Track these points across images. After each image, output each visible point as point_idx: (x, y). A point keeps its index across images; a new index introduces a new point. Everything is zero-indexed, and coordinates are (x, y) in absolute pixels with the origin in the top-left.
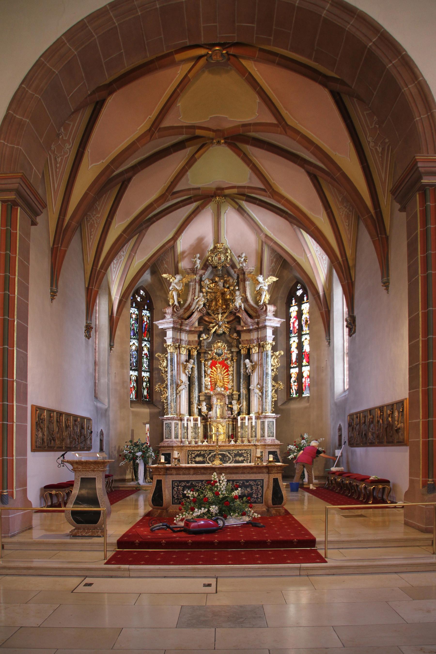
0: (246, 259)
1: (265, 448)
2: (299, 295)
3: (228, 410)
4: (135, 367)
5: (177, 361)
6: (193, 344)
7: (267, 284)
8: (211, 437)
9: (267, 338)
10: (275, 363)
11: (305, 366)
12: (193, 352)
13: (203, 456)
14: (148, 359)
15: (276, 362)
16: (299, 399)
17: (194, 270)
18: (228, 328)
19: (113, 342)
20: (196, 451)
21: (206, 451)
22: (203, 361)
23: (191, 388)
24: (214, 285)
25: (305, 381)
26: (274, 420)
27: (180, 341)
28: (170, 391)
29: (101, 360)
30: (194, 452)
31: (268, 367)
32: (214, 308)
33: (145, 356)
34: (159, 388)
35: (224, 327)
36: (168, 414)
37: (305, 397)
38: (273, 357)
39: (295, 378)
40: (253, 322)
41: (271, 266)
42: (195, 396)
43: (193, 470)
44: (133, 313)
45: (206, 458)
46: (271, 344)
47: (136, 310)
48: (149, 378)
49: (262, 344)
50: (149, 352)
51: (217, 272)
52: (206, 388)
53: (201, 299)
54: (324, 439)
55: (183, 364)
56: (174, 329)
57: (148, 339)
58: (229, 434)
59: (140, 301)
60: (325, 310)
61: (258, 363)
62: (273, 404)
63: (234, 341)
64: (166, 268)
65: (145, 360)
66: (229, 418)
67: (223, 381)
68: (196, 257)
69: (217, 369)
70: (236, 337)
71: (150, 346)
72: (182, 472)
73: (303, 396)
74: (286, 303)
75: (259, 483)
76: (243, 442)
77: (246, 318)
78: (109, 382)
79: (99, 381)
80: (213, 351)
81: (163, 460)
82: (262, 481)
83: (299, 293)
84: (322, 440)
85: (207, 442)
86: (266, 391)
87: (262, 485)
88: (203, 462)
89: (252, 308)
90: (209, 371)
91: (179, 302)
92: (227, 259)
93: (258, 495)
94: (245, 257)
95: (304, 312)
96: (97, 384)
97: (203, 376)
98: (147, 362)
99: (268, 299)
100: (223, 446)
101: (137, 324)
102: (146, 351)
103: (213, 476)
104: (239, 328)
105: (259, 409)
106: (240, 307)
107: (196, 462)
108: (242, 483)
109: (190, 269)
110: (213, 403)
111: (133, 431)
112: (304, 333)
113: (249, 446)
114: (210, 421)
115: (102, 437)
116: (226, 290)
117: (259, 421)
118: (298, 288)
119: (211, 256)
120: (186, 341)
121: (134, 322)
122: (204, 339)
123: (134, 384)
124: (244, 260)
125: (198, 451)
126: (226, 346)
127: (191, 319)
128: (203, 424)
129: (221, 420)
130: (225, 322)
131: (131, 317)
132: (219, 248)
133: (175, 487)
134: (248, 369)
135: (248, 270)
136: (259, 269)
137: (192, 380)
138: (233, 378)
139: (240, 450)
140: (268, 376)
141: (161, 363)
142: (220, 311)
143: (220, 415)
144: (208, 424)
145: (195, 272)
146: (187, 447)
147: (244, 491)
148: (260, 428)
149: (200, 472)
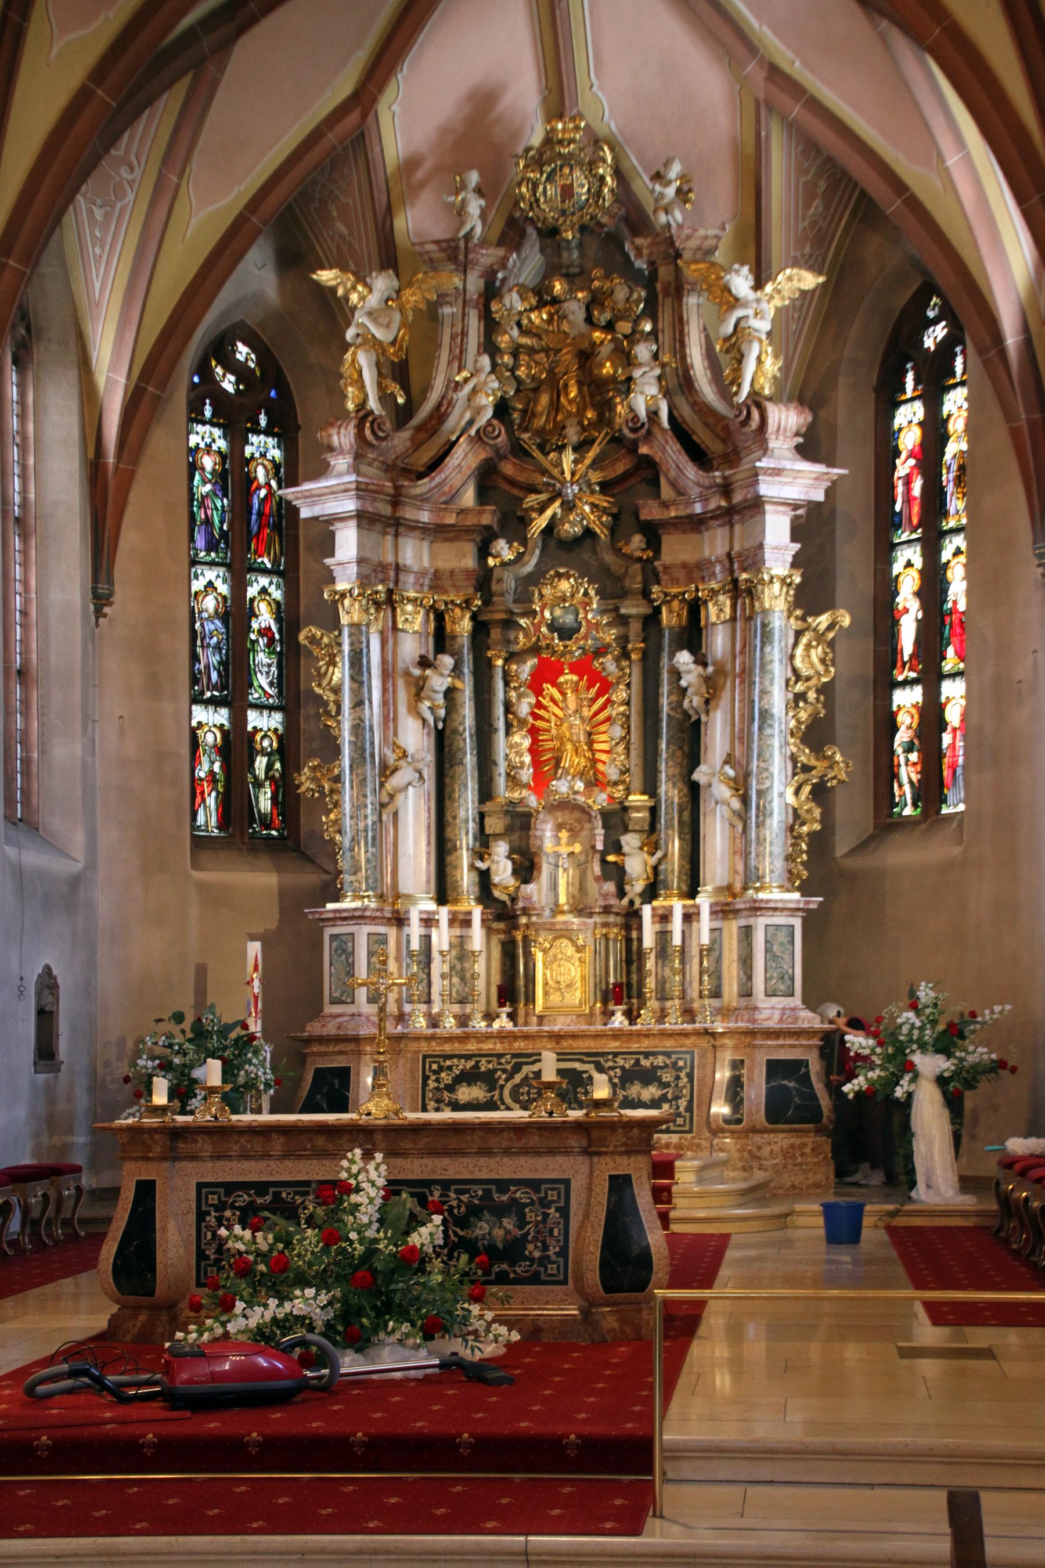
0: (685, 188)
1: (755, 1046)
2: (932, 348)
3: (605, 877)
4: (215, 688)
5: (384, 661)
6: (455, 586)
7: (770, 310)
8: (530, 998)
9: (767, 556)
10: (812, 665)
11: (953, 676)
12: (454, 623)
13: (489, 1079)
14: (274, 652)
15: (815, 660)
16: (923, 826)
17: (457, 248)
18: (604, 511)
19: (110, 582)
20: (459, 1057)
21: (500, 1056)
22: (500, 662)
23: (447, 781)
24: (545, 317)
25: (954, 743)
26: (797, 922)
27: (397, 575)
28: (351, 797)
29: (53, 659)
30: (448, 1063)
31: (772, 683)
32: (547, 421)
33: (262, 642)
34: (314, 779)
35: (587, 508)
36: (337, 898)
37: (950, 817)
38: (804, 640)
39: (910, 733)
40: (707, 482)
41: (804, 217)
42: (462, 814)
43: (282, 1140)
44: (202, 445)
45: (502, 1087)
46: (783, 581)
47: (217, 432)
48: (280, 738)
49: (746, 581)
50: (278, 620)
51: (560, 256)
52: (513, 780)
53: (485, 382)
54: (1008, 1007)
55: (407, 674)
56: (365, 522)
57: (275, 562)
58: (607, 983)
59: (237, 390)
60: (1028, 420)
61: (729, 667)
62: (804, 847)
63: (631, 571)
64: (342, 237)
65: (262, 658)
66: (607, 910)
67: (591, 749)
68: (463, 187)
69: (563, 694)
70: (643, 550)
71: (286, 594)
72: (237, 1148)
73: (945, 810)
74: (876, 390)
75: (552, 1195)
76: (662, 1016)
77: (678, 466)
78: (89, 759)
79: (43, 752)
80: (538, 618)
81: (160, 1098)
82: (562, 1187)
83: (934, 336)
84: (1001, 1012)
85: (512, 1016)
86: (760, 793)
87: (562, 1204)
88: (490, 1105)
89: (711, 420)
90: (524, 709)
91: (385, 398)
92: (599, 194)
93: (545, 1248)
94: (682, 177)
95: (951, 427)
96: (34, 769)
97: (501, 724)
98: (269, 666)
99: (775, 377)
100: (574, 1036)
101: (225, 495)
102: (265, 617)
103: (345, 1163)
104: (651, 512)
105: (736, 872)
106: (653, 415)
107: (456, 1107)
108: (480, 1193)
109: (437, 242)
110: (540, 848)
111: (202, 971)
112: (951, 523)
113: (685, 1034)
114: (527, 926)
115: (50, 998)
116: (597, 335)
117: (732, 928)
118: (931, 314)
119: (529, 180)
120: (423, 573)
121: (208, 487)
122: (503, 564)
123: (212, 763)
124: (679, 191)
125: (468, 1057)
126: (592, 593)
127: (443, 476)
128: (502, 936)
129: (575, 920)
130: (589, 485)
131: (193, 467)
132: (560, 142)
133: (209, 1214)
134: (690, 691)
135: (693, 243)
136: (753, 231)
137: (451, 745)
138: (629, 733)
139: (647, 1055)
140: (771, 726)
141: (323, 670)
142: (573, 434)
143: (570, 896)
144: (519, 938)
145: (461, 257)
146: (417, 1038)
147: (491, 1229)
148: (735, 956)
149: (309, 1146)
